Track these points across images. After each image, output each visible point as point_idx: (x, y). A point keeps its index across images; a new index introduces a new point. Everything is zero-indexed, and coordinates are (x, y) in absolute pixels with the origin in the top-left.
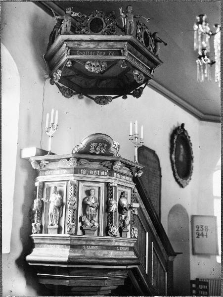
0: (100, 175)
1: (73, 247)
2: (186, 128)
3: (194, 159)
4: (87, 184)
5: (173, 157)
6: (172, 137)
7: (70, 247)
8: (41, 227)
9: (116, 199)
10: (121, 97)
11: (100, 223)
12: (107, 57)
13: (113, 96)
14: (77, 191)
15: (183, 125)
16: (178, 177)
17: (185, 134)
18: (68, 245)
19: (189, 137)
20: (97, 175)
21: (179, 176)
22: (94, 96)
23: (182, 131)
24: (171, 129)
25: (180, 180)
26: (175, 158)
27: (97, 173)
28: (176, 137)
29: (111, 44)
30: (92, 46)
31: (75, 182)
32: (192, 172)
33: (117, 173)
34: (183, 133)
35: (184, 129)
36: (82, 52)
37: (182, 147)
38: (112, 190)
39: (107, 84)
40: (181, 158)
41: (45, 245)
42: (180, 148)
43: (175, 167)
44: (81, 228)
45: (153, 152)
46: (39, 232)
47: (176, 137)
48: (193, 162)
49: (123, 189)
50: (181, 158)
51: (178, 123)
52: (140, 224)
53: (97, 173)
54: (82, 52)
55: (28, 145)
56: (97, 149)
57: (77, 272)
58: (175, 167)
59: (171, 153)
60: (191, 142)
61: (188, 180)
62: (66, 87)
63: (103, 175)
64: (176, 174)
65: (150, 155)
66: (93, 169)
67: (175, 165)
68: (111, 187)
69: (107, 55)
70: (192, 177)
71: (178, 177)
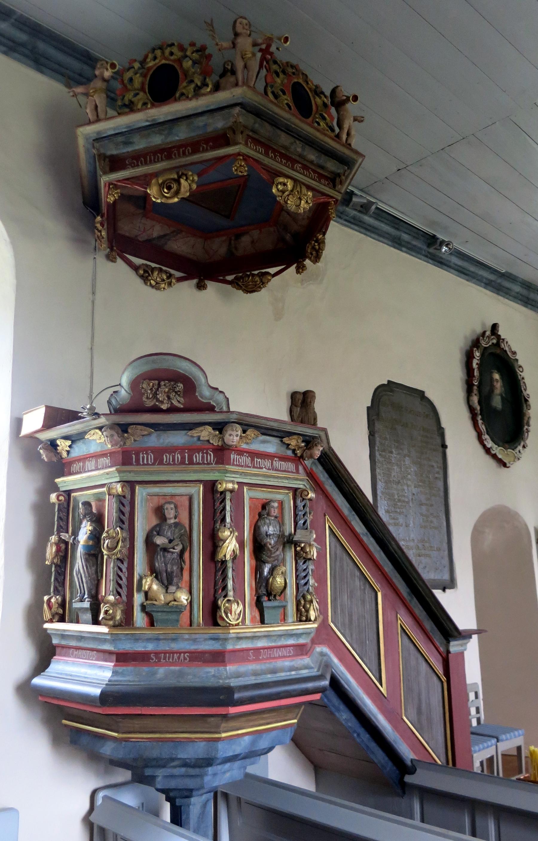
0: (191, 463)
1: (122, 658)
2: (501, 332)
3: (531, 401)
4: (155, 490)
5: (475, 399)
6: (469, 356)
7: (114, 657)
8: (63, 605)
9: (238, 526)
10: (293, 268)
11: (195, 591)
12: (196, 157)
13: (272, 270)
14: (127, 510)
15: (495, 327)
16: (489, 444)
17: (502, 346)
18: (110, 653)
19: (514, 353)
20: (183, 462)
21: (493, 440)
22: (230, 278)
23: (495, 341)
24: (466, 338)
25: (497, 450)
26: (480, 402)
27: (183, 458)
28: (477, 354)
29: (200, 121)
30: (157, 140)
31: (119, 489)
32: (528, 431)
33: (241, 452)
34: (498, 345)
35: (499, 337)
36: (139, 158)
37: (497, 376)
38: (224, 500)
39: (253, 242)
40: (497, 402)
41: (71, 650)
42: (492, 379)
43: (480, 422)
44: (143, 608)
45: (421, 394)
46: (57, 618)
47: (477, 354)
48: (529, 407)
49: (262, 495)
50: (497, 402)
51: (483, 324)
52: (357, 573)
53: (183, 458)
54: (139, 158)
55: (30, 407)
56: (160, 397)
57: (137, 723)
58: (480, 422)
59: (469, 391)
60: (520, 363)
61: (520, 448)
62: (153, 265)
63: (198, 464)
64: (486, 437)
65: (417, 405)
66: (172, 450)
67: (479, 417)
68: (222, 493)
69: (195, 151)
70: (528, 442)
71: (489, 444)
